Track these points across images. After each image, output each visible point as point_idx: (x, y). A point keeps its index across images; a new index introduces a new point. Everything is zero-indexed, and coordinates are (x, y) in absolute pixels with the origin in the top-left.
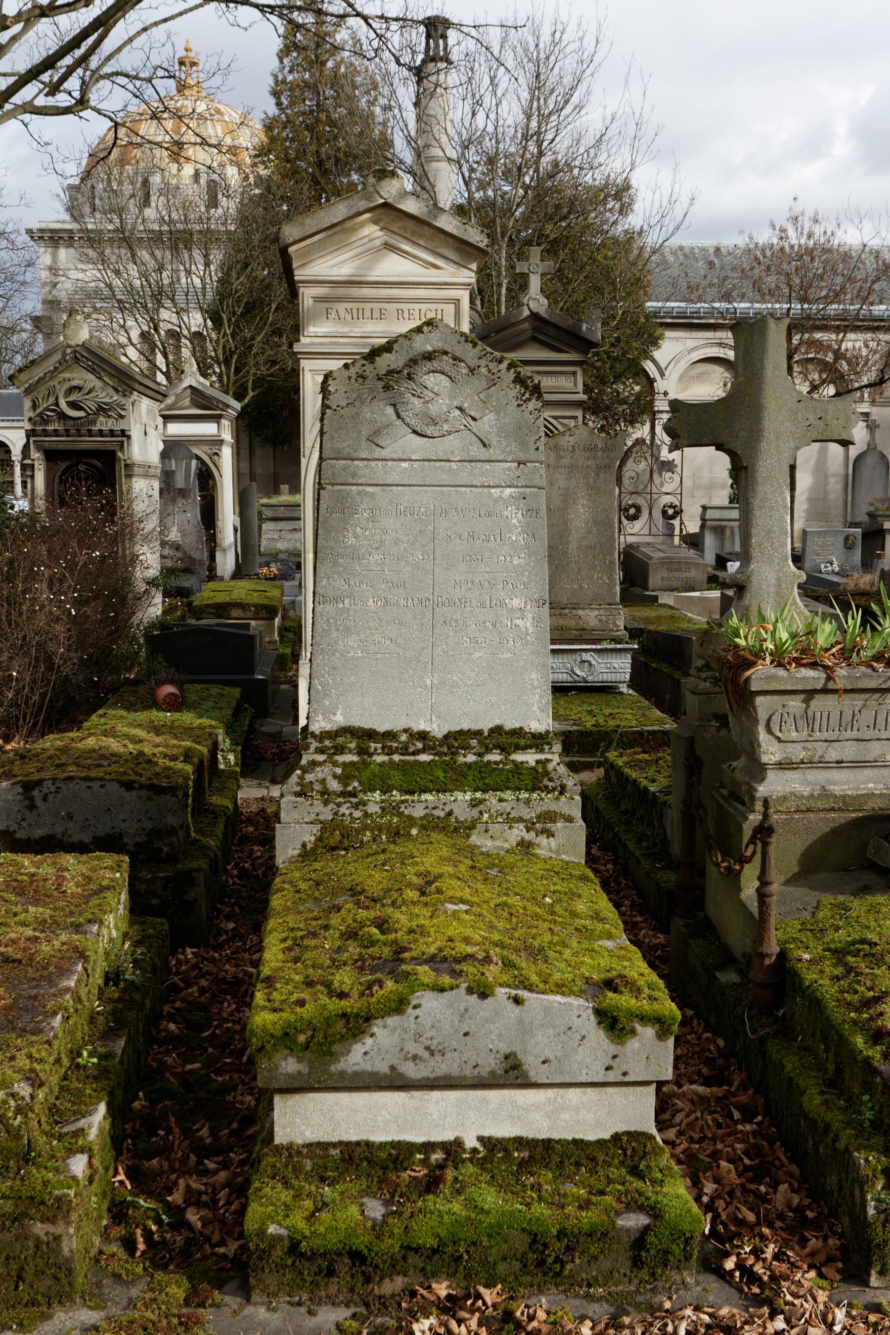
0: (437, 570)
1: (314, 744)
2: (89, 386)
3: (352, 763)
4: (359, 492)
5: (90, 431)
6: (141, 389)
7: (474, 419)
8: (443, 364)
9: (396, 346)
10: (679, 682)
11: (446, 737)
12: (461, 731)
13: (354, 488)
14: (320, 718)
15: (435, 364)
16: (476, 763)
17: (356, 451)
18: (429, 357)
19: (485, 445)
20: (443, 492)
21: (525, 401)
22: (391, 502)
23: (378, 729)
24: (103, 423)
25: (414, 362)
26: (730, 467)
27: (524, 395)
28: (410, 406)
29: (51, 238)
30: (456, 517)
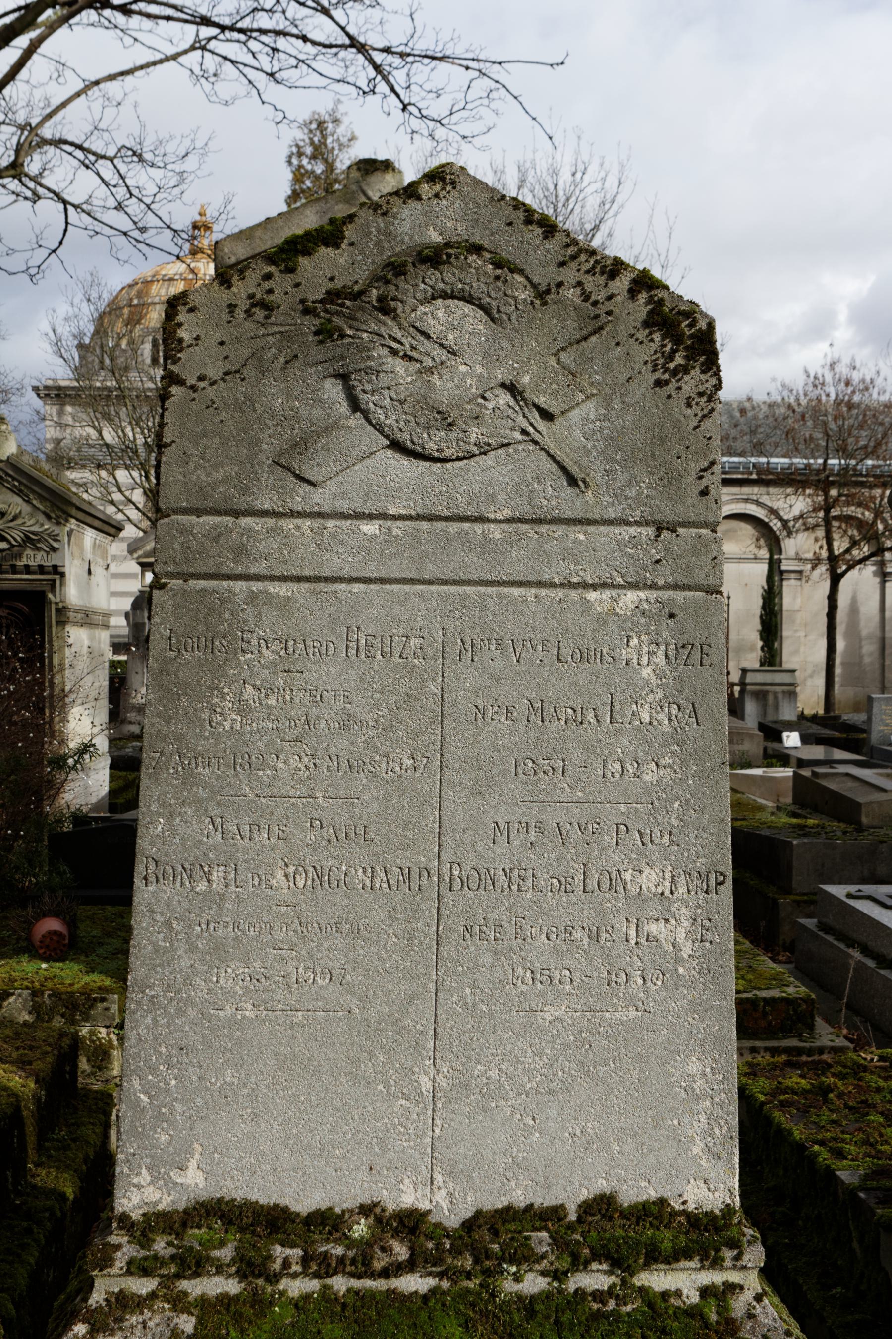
0: (449, 795)
1: (127, 1250)
2: (14, 511)
3: (225, 1300)
4: (252, 597)
5: (13, 567)
6: (80, 515)
7: (547, 416)
8: (470, 276)
9: (350, 232)
10: (775, 901)
11: (469, 1225)
12: (509, 1209)
13: (240, 586)
14: (145, 1177)
15: (450, 276)
16: (546, 1296)
17: (245, 491)
18: (433, 257)
19: (572, 481)
20: (465, 597)
21: (675, 373)
22: (334, 622)
23: (295, 1207)
24: (32, 558)
25: (396, 269)
26: (759, 627)
27: (671, 358)
28: (385, 380)
29: (57, 396)
30: (499, 663)
